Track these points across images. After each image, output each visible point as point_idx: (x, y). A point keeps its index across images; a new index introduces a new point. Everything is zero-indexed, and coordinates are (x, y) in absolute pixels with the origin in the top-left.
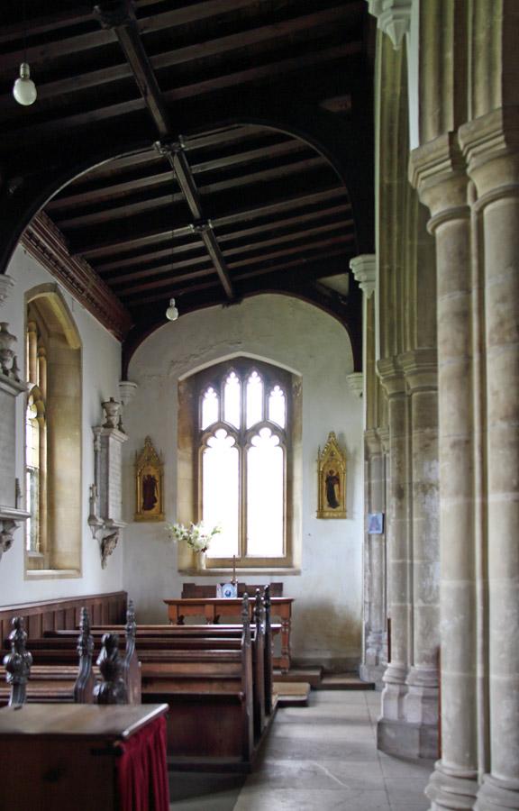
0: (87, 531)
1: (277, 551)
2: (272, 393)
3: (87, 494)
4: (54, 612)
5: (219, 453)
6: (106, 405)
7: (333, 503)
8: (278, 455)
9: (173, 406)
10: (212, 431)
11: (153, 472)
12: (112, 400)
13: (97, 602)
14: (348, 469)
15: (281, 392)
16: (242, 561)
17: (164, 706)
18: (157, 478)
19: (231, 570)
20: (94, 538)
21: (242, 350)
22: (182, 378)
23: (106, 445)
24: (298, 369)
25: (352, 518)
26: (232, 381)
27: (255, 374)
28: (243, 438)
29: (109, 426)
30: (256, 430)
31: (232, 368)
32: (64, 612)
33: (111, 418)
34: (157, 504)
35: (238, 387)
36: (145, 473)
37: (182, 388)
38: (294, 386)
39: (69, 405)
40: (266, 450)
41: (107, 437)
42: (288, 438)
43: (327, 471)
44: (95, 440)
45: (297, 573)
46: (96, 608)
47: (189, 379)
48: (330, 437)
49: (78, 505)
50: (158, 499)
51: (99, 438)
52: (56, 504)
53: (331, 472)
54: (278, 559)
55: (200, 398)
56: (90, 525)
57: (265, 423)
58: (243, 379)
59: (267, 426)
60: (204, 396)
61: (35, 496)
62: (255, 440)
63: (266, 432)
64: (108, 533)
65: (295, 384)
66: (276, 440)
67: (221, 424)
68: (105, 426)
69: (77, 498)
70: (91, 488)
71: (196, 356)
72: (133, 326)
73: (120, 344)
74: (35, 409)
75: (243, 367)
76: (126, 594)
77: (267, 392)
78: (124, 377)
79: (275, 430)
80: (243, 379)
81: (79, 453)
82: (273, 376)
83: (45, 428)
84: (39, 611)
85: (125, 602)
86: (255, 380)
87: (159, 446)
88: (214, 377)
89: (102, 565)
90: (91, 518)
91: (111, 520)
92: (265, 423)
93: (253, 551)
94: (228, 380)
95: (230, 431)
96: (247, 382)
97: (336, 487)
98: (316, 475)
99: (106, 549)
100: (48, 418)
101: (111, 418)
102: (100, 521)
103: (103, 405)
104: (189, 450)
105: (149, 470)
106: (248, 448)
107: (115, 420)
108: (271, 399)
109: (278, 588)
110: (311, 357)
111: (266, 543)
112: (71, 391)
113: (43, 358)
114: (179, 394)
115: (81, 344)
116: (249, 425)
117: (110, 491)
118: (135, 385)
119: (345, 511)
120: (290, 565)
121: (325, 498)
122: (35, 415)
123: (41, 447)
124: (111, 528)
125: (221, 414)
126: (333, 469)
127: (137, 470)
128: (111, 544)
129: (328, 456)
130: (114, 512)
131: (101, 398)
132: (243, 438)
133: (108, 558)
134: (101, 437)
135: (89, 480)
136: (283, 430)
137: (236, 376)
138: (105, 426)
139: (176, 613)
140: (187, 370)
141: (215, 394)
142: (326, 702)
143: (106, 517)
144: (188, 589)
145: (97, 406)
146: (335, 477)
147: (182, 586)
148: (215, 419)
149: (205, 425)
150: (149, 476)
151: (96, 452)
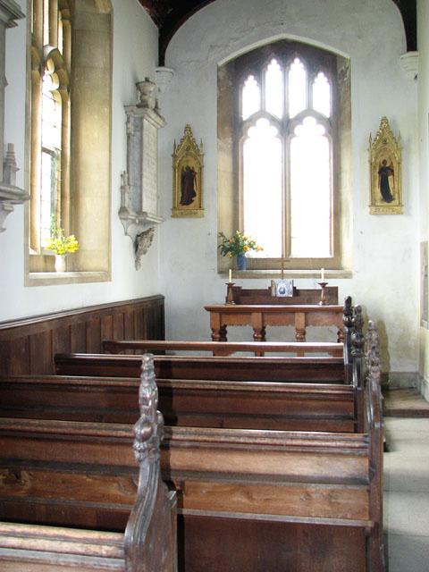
0: (117, 226)
1: (325, 252)
2: (316, 80)
3: (117, 182)
4: (29, 337)
5: (259, 144)
6: (141, 85)
7: (387, 196)
8: (324, 146)
9: (211, 95)
10: (252, 120)
11: (192, 164)
12: (147, 80)
13: (130, 310)
14: (403, 158)
15: (326, 79)
16: (284, 263)
17: (61, 53)
18: (196, 170)
19: (279, 271)
20: (126, 234)
21: (284, 31)
22: (221, 63)
23: (140, 128)
24: (346, 52)
25: (409, 214)
26: (274, 67)
27: (297, 60)
28: (286, 127)
29: (143, 105)
30: (299, 119)
31: (273, 54)
32: (86, 325)
33: (146, 97)
34: (196, 199)
35: (280, 74)
36: (184, 165)
37: (221, 75)
38: (339, 71)
39: (97, 77)
40: (312, 141)
41: (142, 118)
42: (337, 125)
43: (380, 160)
44: (128, 122)
45: (348, 276)
46: (128, 315)
47: (230, 65)
48: (382, 123)
49: (106, 194)
50: (197, 193)
51: (132, 120)
52: (81, 192)
53: (384, 162)
54: (326, 259)
55: (240, 86)
56: (121, 219)
57: (309, 111)
58: (285, 65)
59: (311, 115)
60: (243, 83)
61: (56, 182)
62: (298, 130)
63: (310, 121)
64: (142, 229)
65: (341, 68)
66: (322, 129)
67: (262, 113)
68: (138, 106)
69: (106, 187)
70: (122, 176)
71: (237, 39)
72: (170, 10)
73: (157, 29)
74: (60, 96)
75: (285, 50)
76: (163, 298)
77: (311, 79)
78: (161, 63)
79: (320, 118)
80: (285, 65)
81: (107, 133)
82: (321, 60)
83: (69, 103)
84: (47, 327)
85: (162, 307)
86: (298, 66)
87: (198, 136)
88: (250, 63)
89: (136, 267)
90: (123, 210)
91: (145, 213)
92: (309, 111)
93: (298, 252)
94: (269, 67)
95: (273, 120)
96: (289, 69)
97: (390, 178)
98: (368, 165)
99: (140, 247)
100: (71, 90)
101: (146, 97)
102: (132, 215)
103: (137, 84)
104: (230, 140)
105: (188, 161)
106: (291, 138)
107: (151, 103)
108: (314, 86)
109: (333, 293)
110: (359, 37)
111: (312, 242)
112: (99, 61)
113: (67, 22)
114: (219, 80)
115: (112, 10)
116: (292, 116)
117: (144, 180)
118: (172, 70)
119: (400, 204)
120: (339, 268)
121: (378, 190)
122: (57, 86)
123: (63, 125)
124: (144, 223)
125: (263, 103)
126: (387, 159)
127: (174, 161)
128: (146, 241)
129: (380, 145)
130: (149, 206)
131: (135, 77)
132: (286, 127)
133: (143, 257)
134: (135, 119)
135: (120, 165)
136: (329, 119)
137: (278, 63)
138: (138, 106)
139: (218, 323)
140: (227, 55)
141: (256, 82)
142: (407, 441)
143: (140, 212)
144: (237, 294)
145: (130, 86)
146: (388, 168)
147: (336, 286)
148: (257, 109)
149: (245, 115)
150: (188, 168)
151: (129, 136)
